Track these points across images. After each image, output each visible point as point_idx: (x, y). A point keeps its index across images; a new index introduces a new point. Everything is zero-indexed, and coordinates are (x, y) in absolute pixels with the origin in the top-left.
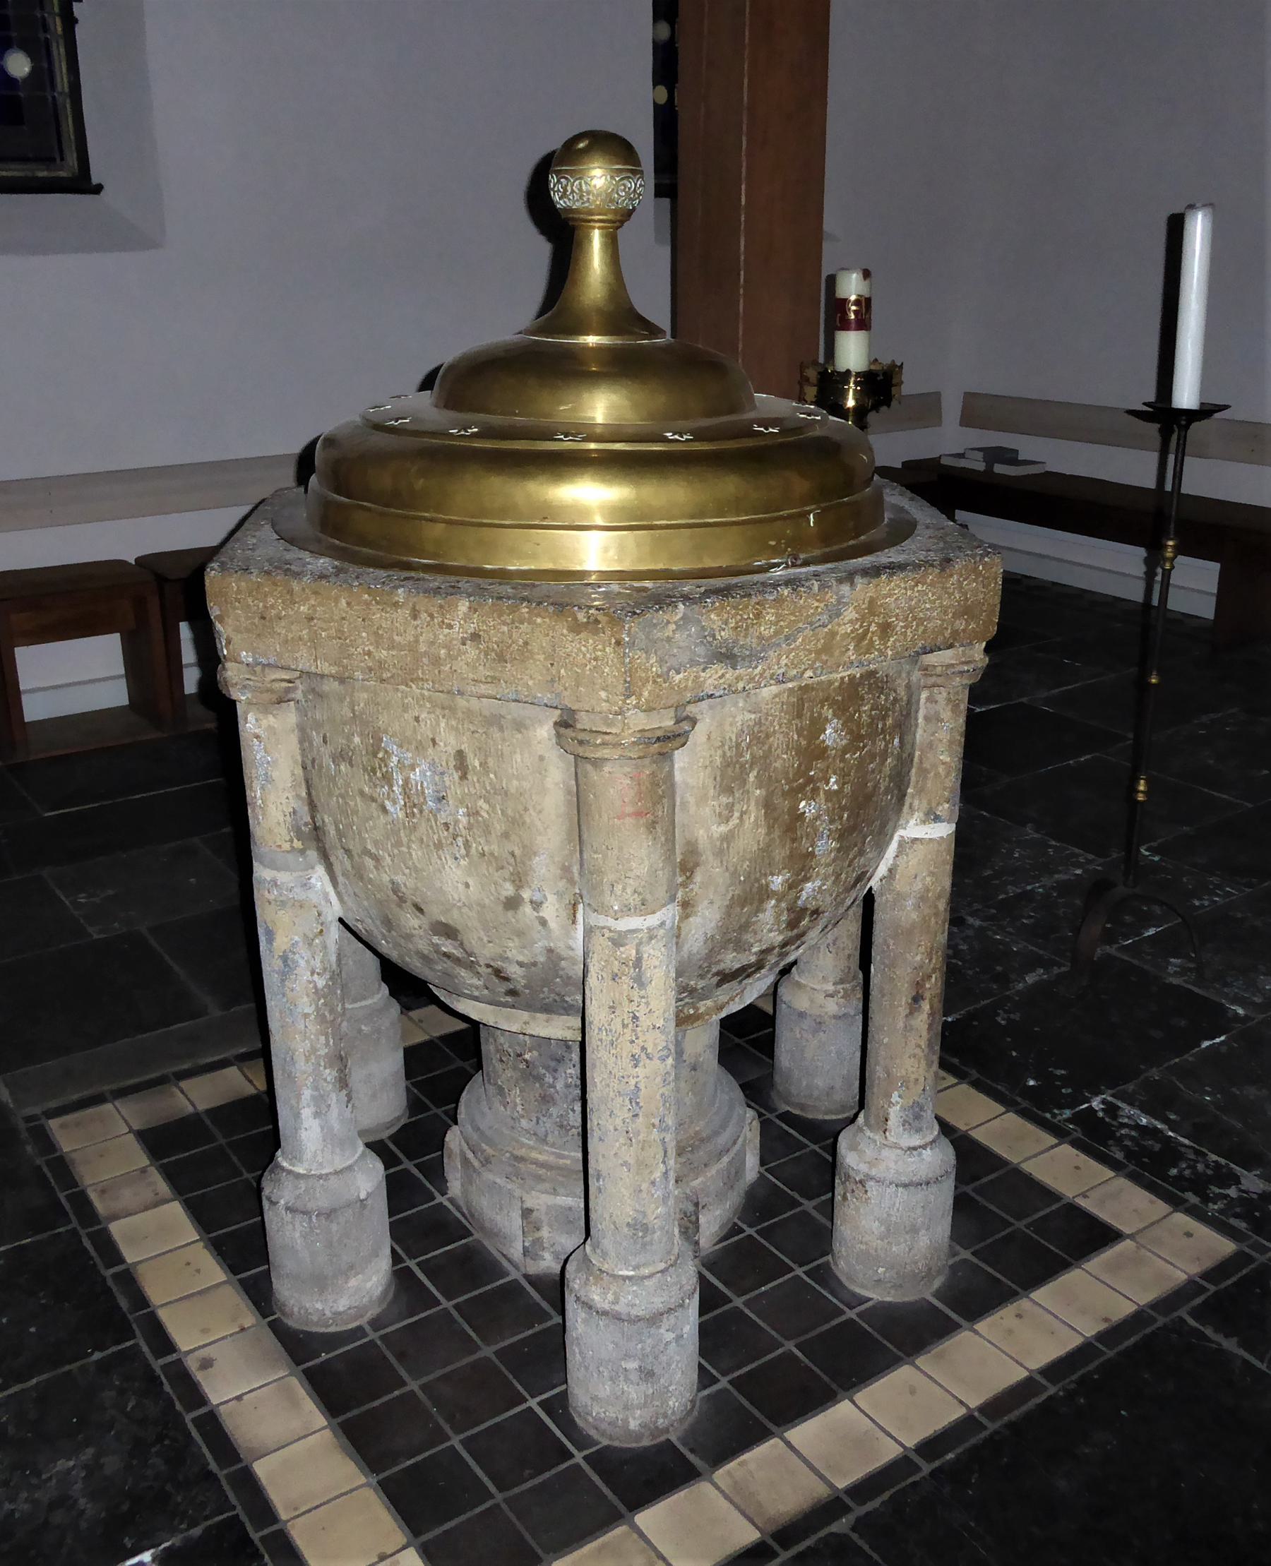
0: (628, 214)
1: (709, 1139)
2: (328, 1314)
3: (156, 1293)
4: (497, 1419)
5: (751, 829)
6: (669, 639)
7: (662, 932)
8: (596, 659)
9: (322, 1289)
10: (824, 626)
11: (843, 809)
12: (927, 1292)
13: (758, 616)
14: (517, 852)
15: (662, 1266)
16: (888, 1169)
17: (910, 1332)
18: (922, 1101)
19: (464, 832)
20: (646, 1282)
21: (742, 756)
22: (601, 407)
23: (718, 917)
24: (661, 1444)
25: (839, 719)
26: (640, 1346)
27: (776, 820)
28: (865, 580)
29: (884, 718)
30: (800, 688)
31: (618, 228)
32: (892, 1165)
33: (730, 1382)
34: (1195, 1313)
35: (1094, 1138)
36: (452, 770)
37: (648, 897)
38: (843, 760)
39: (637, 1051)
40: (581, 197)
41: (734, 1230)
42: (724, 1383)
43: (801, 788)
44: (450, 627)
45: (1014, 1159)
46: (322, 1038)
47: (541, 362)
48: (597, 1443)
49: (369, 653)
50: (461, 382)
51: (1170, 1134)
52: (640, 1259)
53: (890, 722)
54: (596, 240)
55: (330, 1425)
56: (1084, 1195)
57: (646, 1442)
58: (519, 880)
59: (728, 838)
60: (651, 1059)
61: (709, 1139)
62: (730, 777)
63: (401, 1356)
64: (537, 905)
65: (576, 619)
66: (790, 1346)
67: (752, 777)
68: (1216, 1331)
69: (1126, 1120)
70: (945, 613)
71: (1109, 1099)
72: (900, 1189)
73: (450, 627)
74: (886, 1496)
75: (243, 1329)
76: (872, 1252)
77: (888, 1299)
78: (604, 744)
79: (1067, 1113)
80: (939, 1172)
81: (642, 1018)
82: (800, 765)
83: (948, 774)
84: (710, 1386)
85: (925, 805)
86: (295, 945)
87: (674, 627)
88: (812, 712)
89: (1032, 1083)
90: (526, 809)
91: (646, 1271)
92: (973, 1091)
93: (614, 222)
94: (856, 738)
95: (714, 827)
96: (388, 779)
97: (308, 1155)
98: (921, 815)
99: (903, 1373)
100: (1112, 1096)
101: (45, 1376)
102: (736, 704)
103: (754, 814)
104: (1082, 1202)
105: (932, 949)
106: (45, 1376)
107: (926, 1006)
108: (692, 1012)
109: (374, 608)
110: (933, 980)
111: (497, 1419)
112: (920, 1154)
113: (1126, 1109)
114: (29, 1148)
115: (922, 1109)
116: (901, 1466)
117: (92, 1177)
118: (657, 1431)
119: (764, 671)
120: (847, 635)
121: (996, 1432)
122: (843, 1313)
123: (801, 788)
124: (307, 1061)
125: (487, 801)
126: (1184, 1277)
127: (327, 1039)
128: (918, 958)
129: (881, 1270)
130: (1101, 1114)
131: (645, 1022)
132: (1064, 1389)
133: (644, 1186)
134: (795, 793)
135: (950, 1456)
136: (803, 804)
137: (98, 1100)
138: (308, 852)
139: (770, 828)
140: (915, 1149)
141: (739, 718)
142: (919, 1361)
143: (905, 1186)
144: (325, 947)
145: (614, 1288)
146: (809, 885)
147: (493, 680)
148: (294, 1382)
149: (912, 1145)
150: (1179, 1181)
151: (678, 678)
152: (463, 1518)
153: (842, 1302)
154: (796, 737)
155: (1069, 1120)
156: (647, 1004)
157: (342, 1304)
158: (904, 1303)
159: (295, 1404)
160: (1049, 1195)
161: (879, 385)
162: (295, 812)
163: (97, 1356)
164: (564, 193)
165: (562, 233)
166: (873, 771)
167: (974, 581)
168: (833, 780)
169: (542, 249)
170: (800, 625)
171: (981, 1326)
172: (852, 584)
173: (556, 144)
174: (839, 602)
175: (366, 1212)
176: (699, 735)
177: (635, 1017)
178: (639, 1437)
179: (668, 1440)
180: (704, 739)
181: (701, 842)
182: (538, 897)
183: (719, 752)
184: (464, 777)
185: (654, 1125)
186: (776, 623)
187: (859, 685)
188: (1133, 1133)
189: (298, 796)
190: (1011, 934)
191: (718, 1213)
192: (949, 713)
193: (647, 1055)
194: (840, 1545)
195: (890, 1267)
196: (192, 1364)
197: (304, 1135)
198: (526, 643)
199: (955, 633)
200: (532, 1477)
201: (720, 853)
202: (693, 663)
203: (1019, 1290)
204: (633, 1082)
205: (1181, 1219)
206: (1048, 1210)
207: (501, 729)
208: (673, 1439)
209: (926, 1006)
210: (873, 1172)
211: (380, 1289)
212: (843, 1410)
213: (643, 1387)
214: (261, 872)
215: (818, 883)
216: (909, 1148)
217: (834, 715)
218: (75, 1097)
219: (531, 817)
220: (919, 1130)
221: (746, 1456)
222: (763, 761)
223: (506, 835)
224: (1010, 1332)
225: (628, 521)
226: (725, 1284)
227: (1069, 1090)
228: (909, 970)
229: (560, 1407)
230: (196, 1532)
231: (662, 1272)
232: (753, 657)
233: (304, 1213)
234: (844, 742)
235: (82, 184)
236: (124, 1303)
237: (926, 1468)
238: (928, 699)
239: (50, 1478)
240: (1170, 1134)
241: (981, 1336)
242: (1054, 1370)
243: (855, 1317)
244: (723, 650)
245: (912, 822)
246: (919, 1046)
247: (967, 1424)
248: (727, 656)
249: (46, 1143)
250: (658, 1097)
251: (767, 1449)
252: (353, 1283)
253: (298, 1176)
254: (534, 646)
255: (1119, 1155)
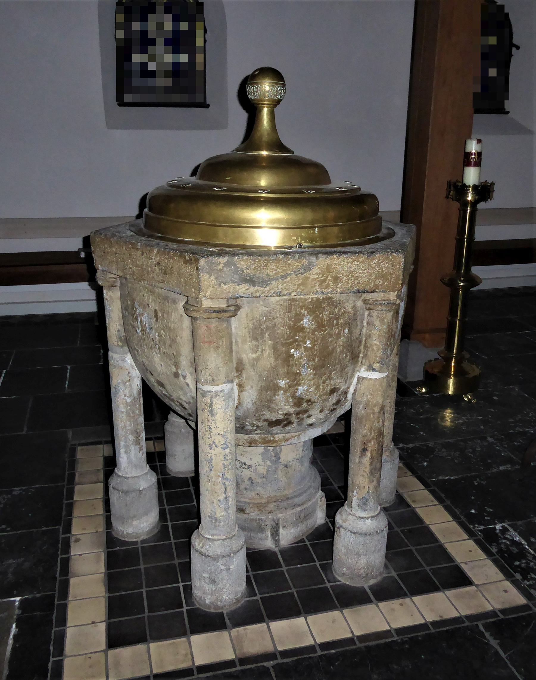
0: (278, 102)
1: (291, 498)
2: (125, 533)
3: (76, 512)
4: (164, 587)
5: (268, 359)
6: (220, 270)
7: (222, 394)
8: (191, 275)
9: (123, 523)
10: (302, 274)
11: (315, 356)
12: (367, 584)
13: (266, 265)
14: (175, 354)
15: (224, 537)
16: (350, 524)
17: (351, 598)
18: (367, 497)
19: (158, 343)
20: (215, 543)
21: (261, 325)
22: (263, 181)
23: (256, 394)
24: (220, 613)
25: (311, 316)
26: (209, 568)
27: (279, 355)
28: (324, 256)
29: (337, 319)
30: (290, 300)
31: (274, 108)
32: (351, 523)
33: (261, 598)
34: (484, 626)
35: (487, 542)
36: (153, 317)
37: (215, 378)
38: (313, 334)
39: (211, 442)
40: (254, 94)
41: (302, 541)
42: (258, 597)
43: (291, 344)
44: (152, 259)
45: (443, 541)
46: (129, 423)
47: (242, 162)
48: (196, 606)
49: (131, 268)
50: (214, 168)
51: (527, 547)
52: (214, 532)
53: (341, 321)
54: (265, 110)
55: (105, 573)
56: (466, 563)
57: (212, 610)
58: (177, 365)
59: (257, 360)
60: (217, 447)
61: (291, 498)
62: (257, 333)
63: (144, 555)
64: (184, 377)
65: (185, 258)
66: (294, 590)
67: (267, 335)
68: (491, 635)
69: (508, 537)
70: (370, 276)
71: (506, 526)
72: (352, 534)
73: (152, 259)
74: (295, 659)
75: (97, 532)
76: (341, 560)
77: (347, 583)
78: (193, 310)
79: (482, 527)
80: (372, 531)
81: (213, 429)
82: (290, 333)
83: (378, 350)
84: (252, 597)
85: (367, 363)
86: (119, 383)
87: (223, 265)
88: (296, 311)
89: (473, 511)
90: (177, 336)
91: (216, 538)
92: (443, 509)
93: (272, 104)
94: (320, 326)
95: (250, 354)
96: (136, 319)
97: (122, 468)
98: (366, 367)
99: (336, 614)
100: (509, 525)
101: (23, 531)
102: (259, 303)
103: (268, 351)
104: (463, 566)
105: (371, 428)
106: (23, 531)
107: (369, 454)
108: (272, 439)
109: (132, 250)
110: (372, 443)
111: (164, 587)
112: (364, 521)
113: (512, 532)
114: (66, 455)
115: (367, 501)
116: (311, 649)
117: (80, 468)
118: (216, 607)
119: (270, 290)
120: (314, 279)
121: (359, 648)
122: (325, 583)
123: (291, 344)
124: (122, 431)
125: (164, 331)
126: (491, 608)
127: (130, 423)
128: (365, 431)
129: (345, 569)
130: (498, 531)
131: (214, 431)
132: (402, 639)
133: (215, 501)
134: (289, 345)
135: (333, 651)
136: (292, 351)
137: (99, 443)
138: (125, 347)
139: (276, 359)
140: (362, 518)
141: (260, 309)
142: (345, 611)
143: (354, 533)
144: (131, 386)
145: (203, 541)
146: (301, 387)
147: (163, 282)
148: (103, 554)
149: (362, 516)
150: (516, 569)
151: (225, 287)
152: (130, 618)
153: (327, 579)
154: (288, 321)
155: (480, 531)
156: (215, 423)
157: (130, 530)
158: (354, 587)
159: (98, 562)
160: (449, 558)
161: (484, 191)
162: (119, 331)
163: (45, 528)
164: (252, 92)
165: (252, 109)
166: (331, 342)
167: (387, 263)
168: (308, 342)
169: (243, 116)
170: (289, 272)
171: (381, 605)
172: (317, 257)
173: (250, 73)
174: (310, 264)
175: (142, 496)
176: (242, 313)
177: (210, 428)
178: (209, 607)
179: (222, 612)
180: (245, 316)
181: (244, 359)
182: (184, 374)
183: (251, 322)
184: (157, 321)
185: (219, 476)
186: (276, 270)
187: (321, 302)
188: (508, 543)
189: (120, 325)
190: (505, 448)
191: (292, 531)
192: (378, 323)
193: (216, 446)
194: (266, 671)
195: (348, 569)
196: (73, 539)
197: (121, 459)
198: (172, 267)
199: (376, 286)
200: (163, 611)
201: (253, 366)
202: (233, 282)
203: (408, 594)
204: (209, 455)
205: (507, 584)
206: (444, 565)
207: (168, 302)
208: (225, 612)
209: (369, 454)
210: (344, 524)
211: (148, 529)
212: (301, 620)
213: (211, 586)
214: (110, 354)
215: (305, 388)
216: (360, 517)
217: (308, 313)
218: (92, 441)
219: (178, 339)
220: (366, 510)
221: (249, 627)
222: (272, 329)
223: (170, 346)
224: (393, 610)
225: (276, 226)
226: (284, 560)
227: (489, 518)
228: (361, 437)
229: (188, 589)
230: (38, 595)
231: (223, 540)
232: (264, 283)
233: (117, 490)
234: (314, 326)
235: (204, 105)
236: (64, 513)
237: (319, 653)
238: (368, 315)
239: (5, 564)
240: (527, 547)
241: (379, 609)
242: (400, 631)
243: (329, 587)
244: (248, 278)
245: (362, 369)
246: (365, 472)
247: (350, 641)
248: (251, 281)
249: (73, 452)
250: (221, 464)
251: (261, 626)
252: (135, 523)
253: (119, 476)
254: (174, 269)
255: (494, 550)
